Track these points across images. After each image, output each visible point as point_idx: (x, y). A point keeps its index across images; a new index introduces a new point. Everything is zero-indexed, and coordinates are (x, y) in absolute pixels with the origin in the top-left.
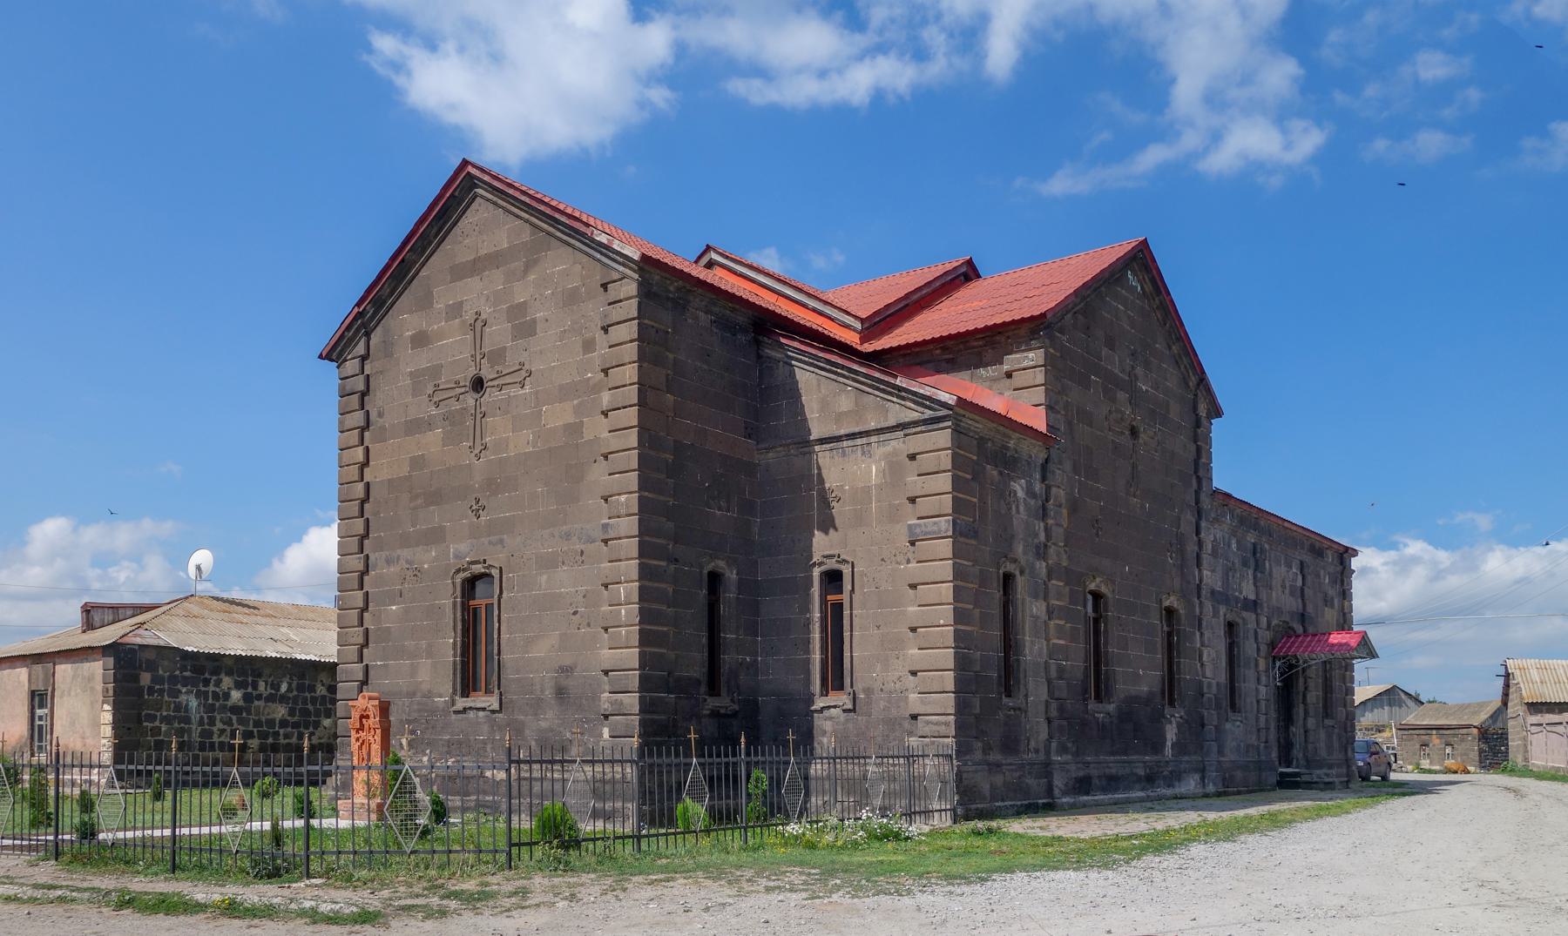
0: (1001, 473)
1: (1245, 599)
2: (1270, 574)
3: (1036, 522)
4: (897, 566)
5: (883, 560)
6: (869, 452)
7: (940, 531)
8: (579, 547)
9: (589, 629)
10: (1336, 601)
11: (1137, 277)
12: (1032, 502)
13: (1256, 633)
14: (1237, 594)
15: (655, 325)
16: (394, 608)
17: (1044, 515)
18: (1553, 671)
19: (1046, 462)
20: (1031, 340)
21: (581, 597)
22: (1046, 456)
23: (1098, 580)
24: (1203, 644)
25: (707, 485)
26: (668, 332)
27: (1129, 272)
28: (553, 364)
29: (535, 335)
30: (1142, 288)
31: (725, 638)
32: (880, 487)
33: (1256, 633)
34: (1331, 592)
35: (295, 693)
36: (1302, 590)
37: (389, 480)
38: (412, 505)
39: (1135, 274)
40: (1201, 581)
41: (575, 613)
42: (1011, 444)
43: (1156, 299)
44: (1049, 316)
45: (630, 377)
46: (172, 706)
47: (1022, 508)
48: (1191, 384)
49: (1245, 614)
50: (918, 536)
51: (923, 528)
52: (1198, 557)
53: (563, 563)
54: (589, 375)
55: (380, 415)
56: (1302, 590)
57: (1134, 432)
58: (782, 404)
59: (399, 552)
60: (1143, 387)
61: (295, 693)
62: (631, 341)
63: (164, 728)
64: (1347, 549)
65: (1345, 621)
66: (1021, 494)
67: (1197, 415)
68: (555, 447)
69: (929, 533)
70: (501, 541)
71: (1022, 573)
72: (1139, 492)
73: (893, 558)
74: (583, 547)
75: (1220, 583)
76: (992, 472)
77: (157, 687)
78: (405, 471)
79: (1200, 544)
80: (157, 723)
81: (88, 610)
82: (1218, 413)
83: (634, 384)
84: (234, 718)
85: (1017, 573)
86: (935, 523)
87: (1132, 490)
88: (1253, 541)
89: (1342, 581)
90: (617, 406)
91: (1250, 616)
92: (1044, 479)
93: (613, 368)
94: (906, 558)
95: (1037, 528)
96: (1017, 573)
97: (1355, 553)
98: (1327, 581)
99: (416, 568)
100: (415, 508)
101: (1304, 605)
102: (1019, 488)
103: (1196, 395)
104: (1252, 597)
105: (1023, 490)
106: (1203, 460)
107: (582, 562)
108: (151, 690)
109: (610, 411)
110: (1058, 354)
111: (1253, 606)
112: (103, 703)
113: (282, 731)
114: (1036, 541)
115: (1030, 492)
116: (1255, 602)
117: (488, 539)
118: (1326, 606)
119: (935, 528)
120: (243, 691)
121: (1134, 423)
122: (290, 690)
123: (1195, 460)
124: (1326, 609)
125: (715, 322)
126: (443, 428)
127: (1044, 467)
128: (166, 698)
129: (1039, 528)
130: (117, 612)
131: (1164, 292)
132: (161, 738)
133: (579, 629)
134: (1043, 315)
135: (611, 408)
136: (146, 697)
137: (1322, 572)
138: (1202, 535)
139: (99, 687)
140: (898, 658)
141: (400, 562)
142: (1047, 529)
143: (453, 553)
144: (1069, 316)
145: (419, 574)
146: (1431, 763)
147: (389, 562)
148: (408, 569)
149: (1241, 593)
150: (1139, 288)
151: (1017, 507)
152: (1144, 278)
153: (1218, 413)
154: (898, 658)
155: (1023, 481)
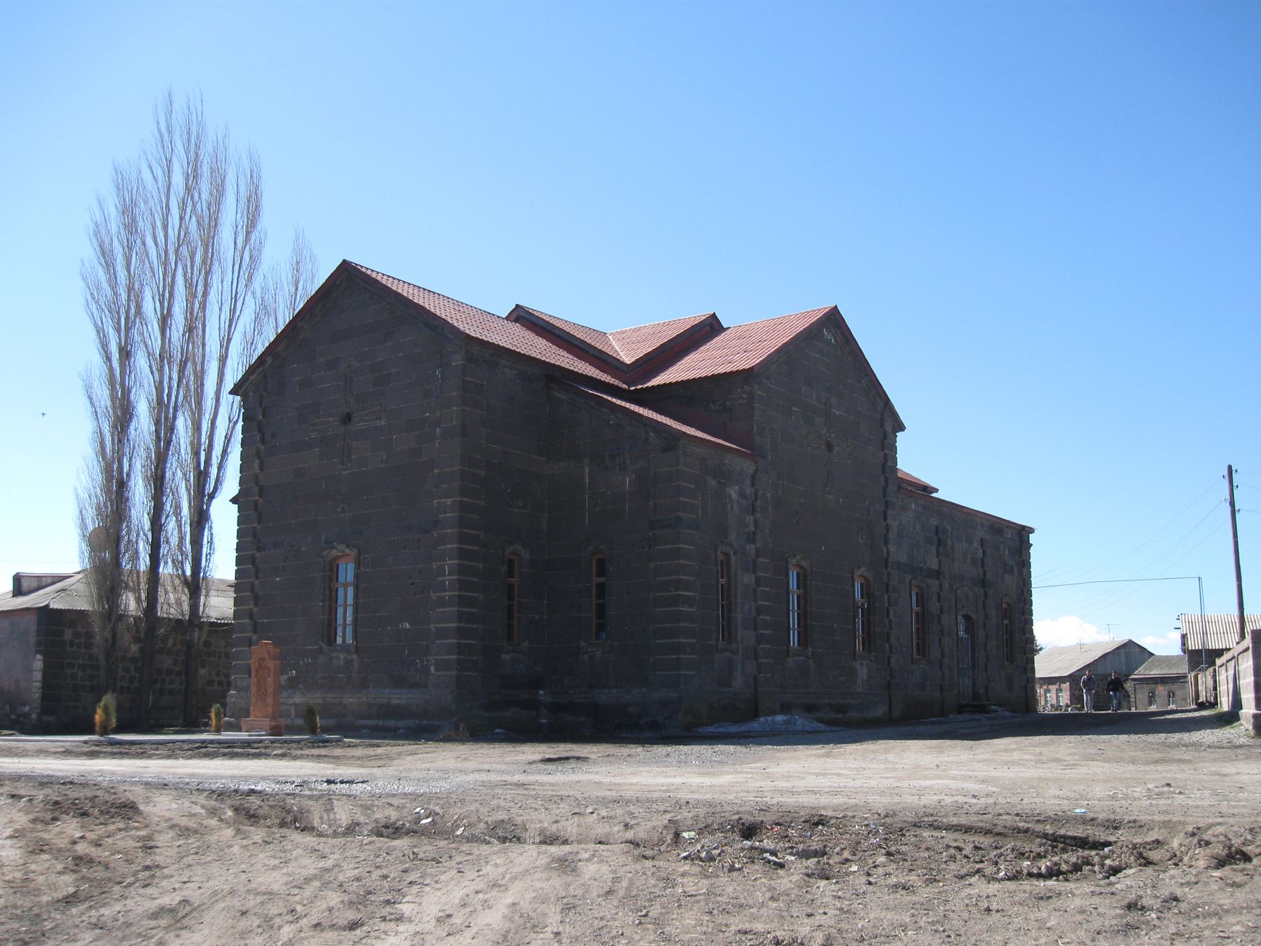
0: (719, 482)
1: (929, 569)
2: (952, 548)
3: (747, 516)
10: (1016, 569)
11: (831, 332)
12: (744, 502)
13: (939, 595)
14: (921, 565)
15: (474, 380)
16: (278, 579)
17: (753, 510)
18: (1250, 623)
19: (755, 472)
20: (744, 385)
22: (755, 468)
23: (798, 557)
24: (890, 604)
25: (509, 491)
26: (483, 385)
27: (825, 330)
28: (402, 406)
30: (835, 340)
31: (194, 631)
33: (939, 595)
34: (1011, 562)
35: (179, 647)
36: (982, 561)
39: (829, 330)
40: (888, 555)
41: (413, 584)
42: (727, 461)
43: (847, 347)
44: (755, 369)
46: (87, 656)
47: (735, 507)
48: (879, 408)
49: (929, 581)
52: (886, 537)
53: (405, 547)
55: (273, 436)
56: (982, 561)
57: (830, 447)
60: (837, 413)
61: (179, 647)
63: (80, 674)
64: (1024, 527)
65: (1024, 585)
66: (734, 496)
67: (884, 430)
71: (735, 553)
72: (833, 491)
75: (905, 557)
76: (712, 482)
77: (77, 641)
79: (888, 528)
80: (75, 670)
81: (18, 579)
82: (901, 427)
84: (132, 667)
85: (732, 554)
87: (827, 489)
88: (936, 523)
89: (1021, 554)
91: (934, 584)
92: (753, 485)
95: (747, 520)
96: (732, 554)
98: (1007, 553)
101: (985, 573)
102: (733, 492)
103: (882, 415)
104: (935, 567)
105: (736, 492)
106: (889, 464)
107: (419, 547)
108: (72, 644)
110: (765, 395)
111: (937, 574)
112: (37, 652)
113: (167, 678)
114: (747, 530)
115: (742, 495)
116: (938, 572)
118: (1006, 572)
120: (140, 645)
121: (829, 439)
122: (174, 645)
123: (883, 464)
124: (1006, 576)
125: (517, 375)
127: (753, 477)
128: (82, 650)
129: (749, 520)
130: (41, 582)
132: (77, 682)
134: (751, 369)
136: (68, 649)
137: (1002, 546)
138: (889, 521)
139: (32, 640)
142: (756, 522)
144: (774, 366)
146: (1177, 706)
149: (925, 564)
150: (833, 340)
151: (732, 506)
152: (837, 333)
153: (901, 427)
155: (737, 487)
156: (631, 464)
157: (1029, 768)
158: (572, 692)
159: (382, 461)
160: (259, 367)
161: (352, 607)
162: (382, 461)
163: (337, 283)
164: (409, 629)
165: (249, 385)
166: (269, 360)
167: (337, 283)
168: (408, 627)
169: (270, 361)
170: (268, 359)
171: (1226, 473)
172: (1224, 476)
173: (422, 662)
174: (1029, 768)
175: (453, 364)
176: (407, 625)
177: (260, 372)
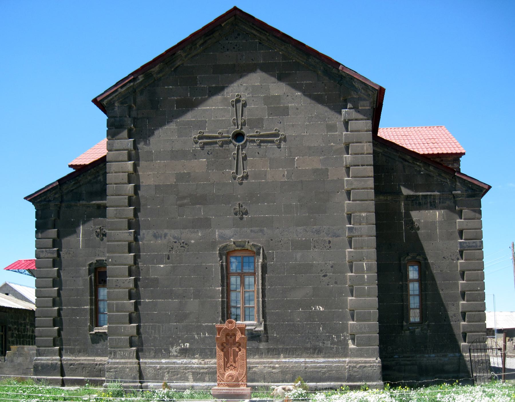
4: (452, 261)
5: (444, 257)
6: (435, 205)
7: (477, 246)
8: (327, 239)
9: (336, 285)
16: (162, 266)
20: (454, 163)
21: (329, 267)
29: (288, 115)
32: (440, 222)
37: (156, 186)
38: (178, 202)
45: (367, 150)
50: (465, 247)
51: (468, 244)
53: (315, 247)
54: (332, 144)
58: (382, 175)
59: (166, 231)
62: (367, 131)
68: (306, 181)
69: (471, 247)
70: (262, 231)
73: (450, 257)
74: (330, 239)
78: (172, 180)
83: (370, 154)
86: (474, 242)
90: (357, 164)
93: (353, 143)
94: (457, 257)
97: (106, 237)
99: (183, 243)
100: (181, 206)
109: (352, 166)
117: (250, 228)
119: (474, 244)
126: (207, 159)
131: (111, 127)
133: (328, 285)
135: (353, 164)
140: (453, 305)
141: (167, 238)
143: (218, 235)
145: (186, 246)
147: (155, 236)
148: (175, 242)
154: (453, 305)
156: (440, 202)
157: (224, 384)
158: (396, 356)
159: (284, 175)
160: (132, 82)
161: (411, 292)
162: (284, 175)
163: (223, 25)
164: (323, 311)
165: (116, 96)
166: (141, 78)
167: (223, 25)
168: (321, 310)
169: (141, 80)
170: (140, 77)
171: (511, 246)
172: (510, 247)
173: (338, 337)
174: (224, 384)
175: (360, 108)
176: (321, 308)
177: (130, 87)
